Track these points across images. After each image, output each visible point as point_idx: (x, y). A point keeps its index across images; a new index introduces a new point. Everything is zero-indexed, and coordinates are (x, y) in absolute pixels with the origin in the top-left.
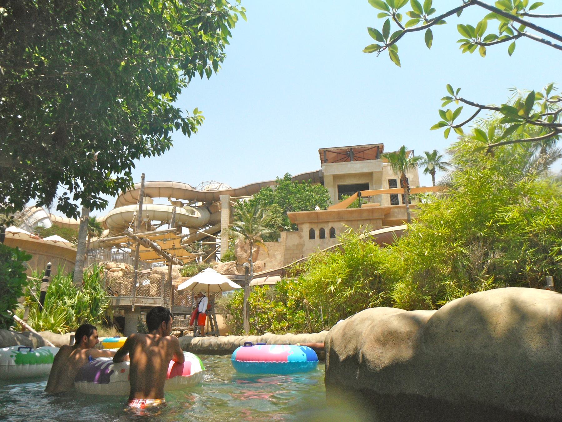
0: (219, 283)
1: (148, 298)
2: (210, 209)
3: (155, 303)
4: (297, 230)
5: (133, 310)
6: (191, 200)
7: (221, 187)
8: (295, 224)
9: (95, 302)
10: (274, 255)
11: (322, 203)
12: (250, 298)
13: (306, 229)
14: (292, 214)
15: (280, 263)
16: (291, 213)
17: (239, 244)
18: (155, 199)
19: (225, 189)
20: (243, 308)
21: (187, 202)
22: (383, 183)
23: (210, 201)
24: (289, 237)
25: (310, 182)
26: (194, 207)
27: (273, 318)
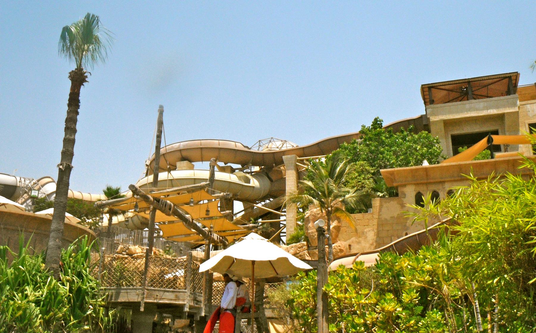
0: (270, 259)
1: (165, 291)
2: (270, 174)
3: (177, 298)
4: (397, 195)
5: (142, 309)
6: (245, 165)
7: (285, 145)
8: (392, 188)
9: (79, 298)
10: (363, 233)
11: (433, 158)
12: (328, 286)
13: (410, 192)
14: (387, 172)
15: (372, 244)
16: (385, 170)
17: (311, 218)
18: (196, 164)
19: (290, 147)
20: (315, 307)
21: (239, 166)
22: (520, 129)
23: (270, 164)
24: (385, 205)
25: (411, 131)
26: (248, 173)
27: (374, 324)
